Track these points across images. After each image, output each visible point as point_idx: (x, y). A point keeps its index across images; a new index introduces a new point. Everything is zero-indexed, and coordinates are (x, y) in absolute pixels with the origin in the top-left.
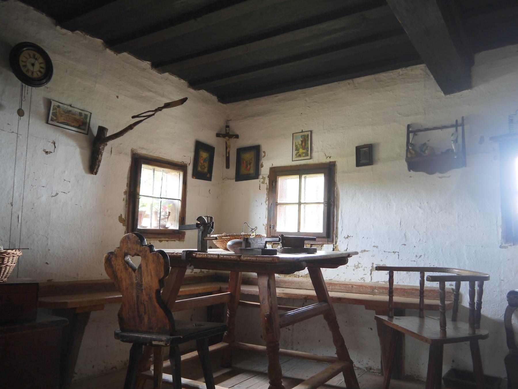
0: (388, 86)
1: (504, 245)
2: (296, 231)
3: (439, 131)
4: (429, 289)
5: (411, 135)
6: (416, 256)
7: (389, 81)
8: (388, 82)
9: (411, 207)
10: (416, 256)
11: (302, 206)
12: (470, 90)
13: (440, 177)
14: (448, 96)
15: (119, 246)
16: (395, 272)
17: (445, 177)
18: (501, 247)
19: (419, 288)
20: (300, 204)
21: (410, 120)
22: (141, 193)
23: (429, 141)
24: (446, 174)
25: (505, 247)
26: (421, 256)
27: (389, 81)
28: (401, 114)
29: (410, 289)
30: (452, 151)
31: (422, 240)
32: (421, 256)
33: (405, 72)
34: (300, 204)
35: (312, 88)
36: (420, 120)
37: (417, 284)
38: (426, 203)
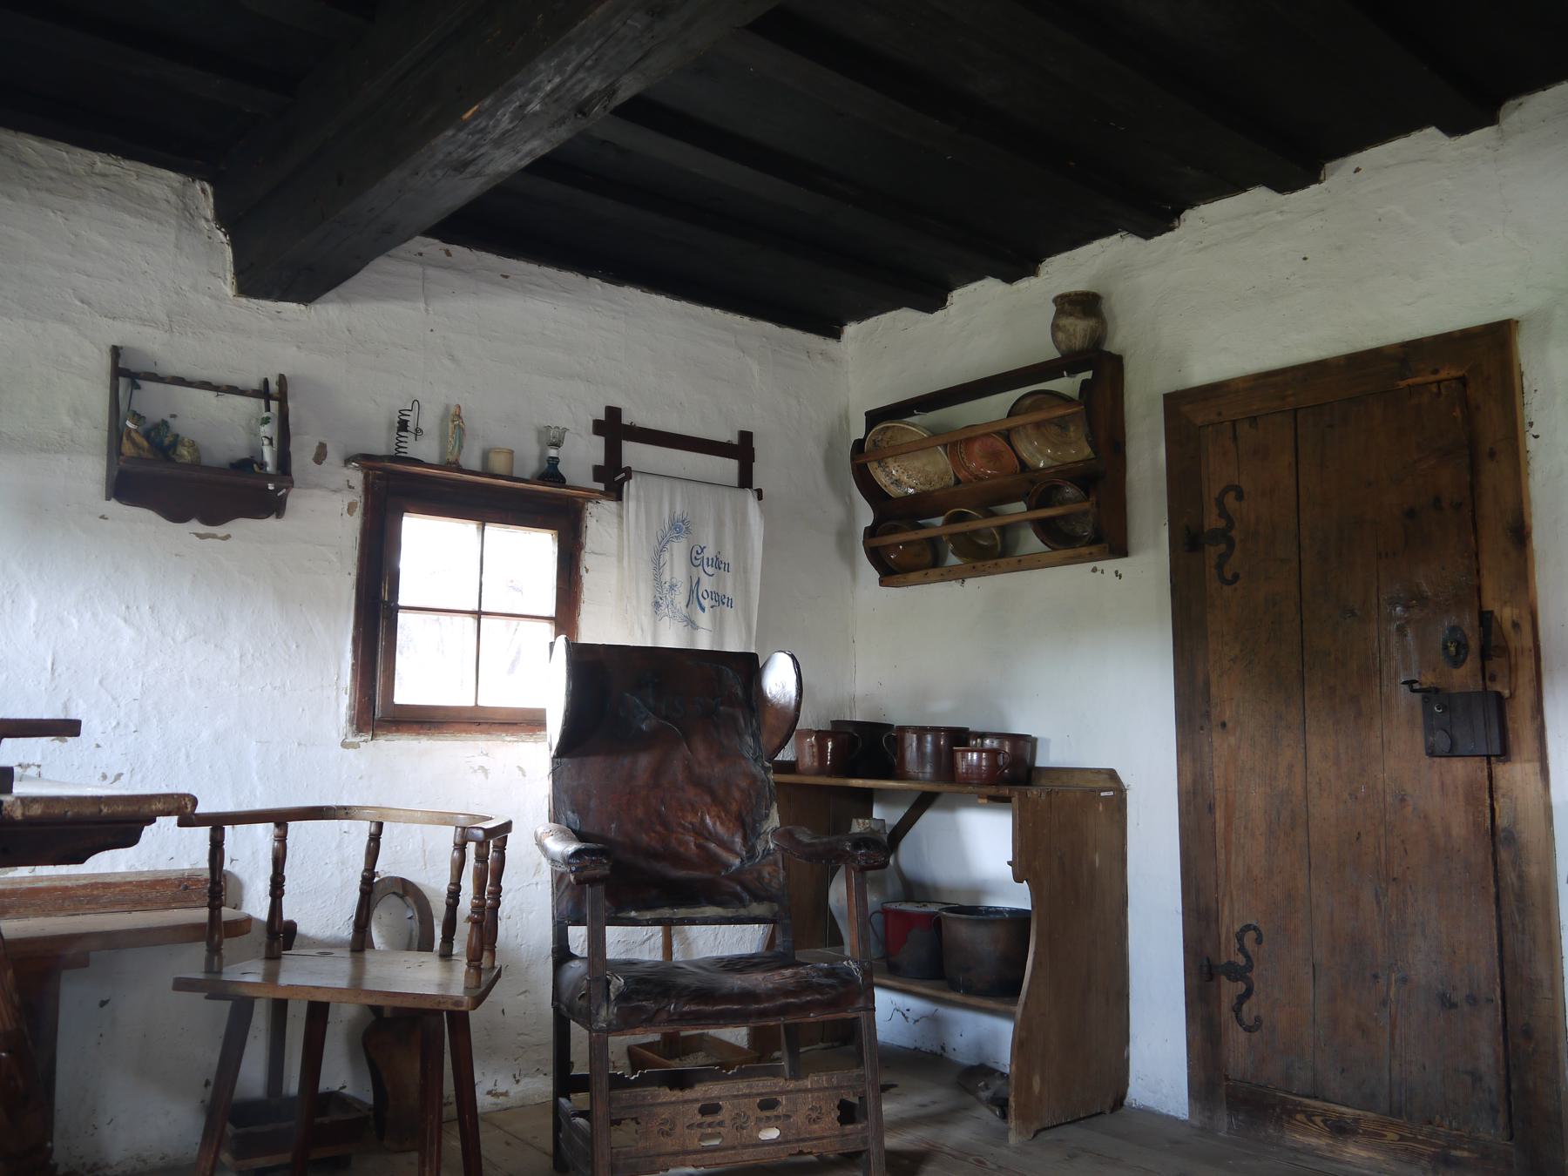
0: (49, 190)
1: (351, 739)
2: (471, 703)
3: (211, 395)
4: (151, 878)
5: (123, 381)
6: (104, 777)
7: (54, 174)
8: (51, 179)
9: (94, 615)
10: (104, 777)
11: (484, 620)
12: (302, 307)
13: (198, 535)
14: (243, 300)
15: (1050, 756)
16: (228, 828)
17: (214, 536)
18: (344, 745)
19: (207, 875)
20: (478, 614)
21: (124, 333)
22: (493, 530)
23: (174, 416)
24: (219, 530)
25: (355, 746)
26: (119, 776)
27: (54, 174)
28: (89, 304)
29: (85, 887)
30: (263, 465)
31: (126, 726)
32: (119, 776)
33: (114, 169)
34: (478, 614)
35: (662, 301)
36: (153, 344)
37: (202, 862)
38: (145, 608)
